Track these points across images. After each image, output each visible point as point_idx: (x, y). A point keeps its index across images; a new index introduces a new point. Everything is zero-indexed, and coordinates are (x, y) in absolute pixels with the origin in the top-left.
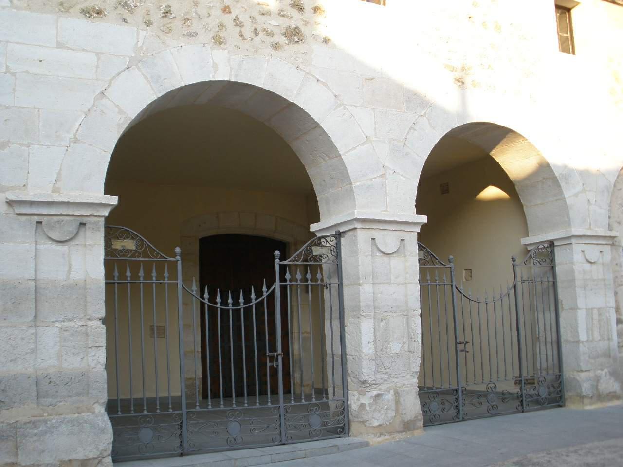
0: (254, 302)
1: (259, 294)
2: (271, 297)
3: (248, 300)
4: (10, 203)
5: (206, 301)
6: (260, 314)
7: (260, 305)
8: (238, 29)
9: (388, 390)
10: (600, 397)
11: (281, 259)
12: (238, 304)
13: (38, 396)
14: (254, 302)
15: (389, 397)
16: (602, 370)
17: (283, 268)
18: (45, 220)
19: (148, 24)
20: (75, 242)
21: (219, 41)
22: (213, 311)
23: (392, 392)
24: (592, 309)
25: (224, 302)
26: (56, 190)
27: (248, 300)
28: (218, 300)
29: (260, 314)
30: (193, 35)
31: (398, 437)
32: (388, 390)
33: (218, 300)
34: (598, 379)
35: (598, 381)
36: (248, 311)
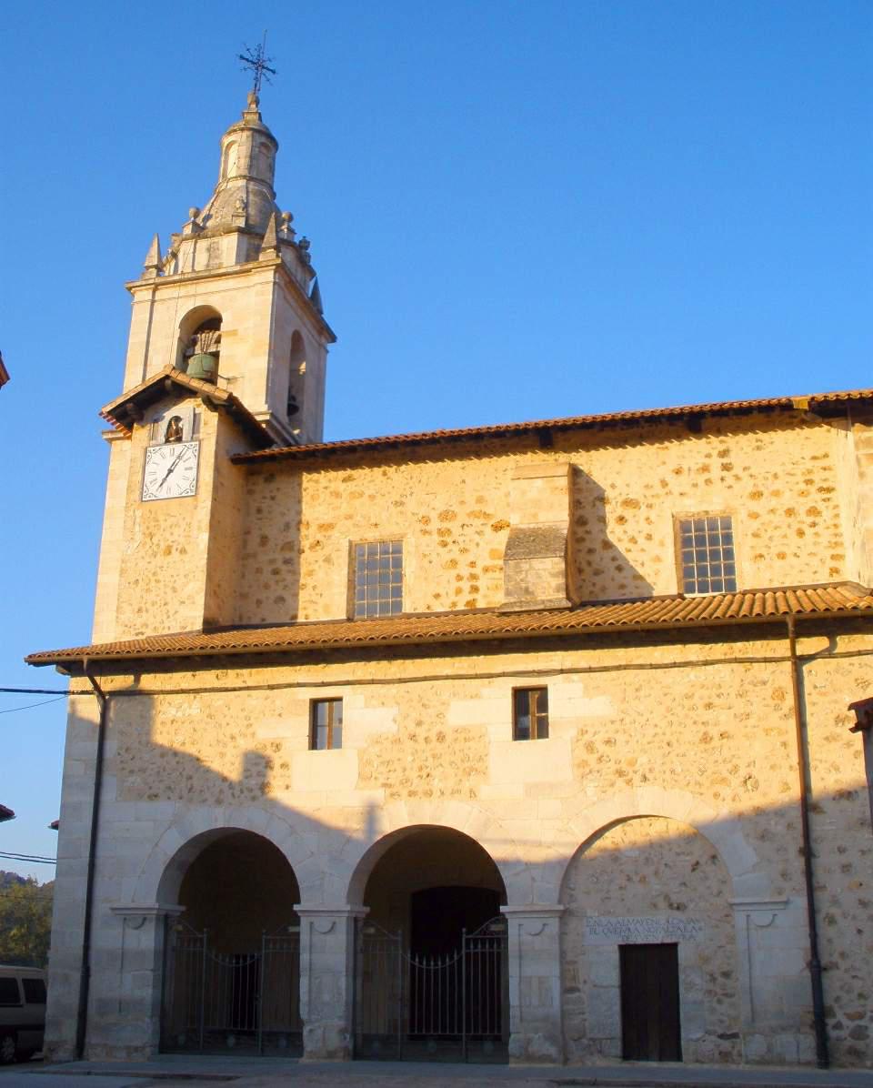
0: (448, 964)
1: (452, 958)
2: (460, 961)
3: (444, 962)
4: (113, 909)
5: (417, 964)
6: (452, 974)
7: (452, 966)
8: (231, 791)
9: (319, 1027)
10: (530, 1058)
11: (468, 933)
12: (430, 965)
13: (120, 1011)
14: (448, 964)
15: (320, 1032)
16: (536, 1033)
17: (468, 941)
18: (128, 917)
19: (181, 798)
20: (143, 928)
21: (219, 802)
22: (421, 970)
23: (322, 1029)
24: (531, 977)
25: (428, 965)
26: (133, 901)
27: (444, 962)
28: (425, 963)
29: (452, 974)
30: (204, 801)
31: (322, 1061)
32: (319, 1027)
33: (425, 963)
34: (529, 1041)
35: (528, 1044)
36: (245, 968)
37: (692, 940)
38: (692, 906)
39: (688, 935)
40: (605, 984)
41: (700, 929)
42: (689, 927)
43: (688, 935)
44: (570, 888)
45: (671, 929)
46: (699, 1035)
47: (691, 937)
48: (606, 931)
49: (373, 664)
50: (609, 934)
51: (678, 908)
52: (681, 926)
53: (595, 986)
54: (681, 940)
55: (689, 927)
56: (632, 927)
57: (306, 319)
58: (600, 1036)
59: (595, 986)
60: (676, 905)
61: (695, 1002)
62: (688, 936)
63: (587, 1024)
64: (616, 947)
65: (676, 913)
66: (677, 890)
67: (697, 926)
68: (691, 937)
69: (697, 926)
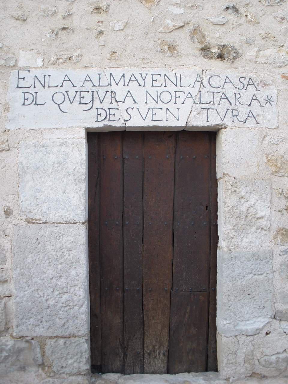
37: (251, 123)
38: (250, 53)
39: (243, 112)
40: (53, 217)
41: (269, 101)
42: (246, 95)
43: (243, 112)
44: (246, 352)
45: (206, 98)
46: (259, 323)
47: (251, 115)
48: (59, 98)
49: (97, 127)
50: (66, 106)
51: (221, 57)
52: (230, 91)
53: (30, 222)
54: (227, 121)
55: (246, 95)
56: (120, 92)
57: (86, 296)
58: (40, 331)
59: (30, 222)
60: (215, 50)
61: (256, 256)
62: (243, 116)
63: (11, 303)
64: (83, 134)
65: (217, 64)
66: (220, 20)
67: (262, 95)
68: (251, 115)
69: (262, 95)
